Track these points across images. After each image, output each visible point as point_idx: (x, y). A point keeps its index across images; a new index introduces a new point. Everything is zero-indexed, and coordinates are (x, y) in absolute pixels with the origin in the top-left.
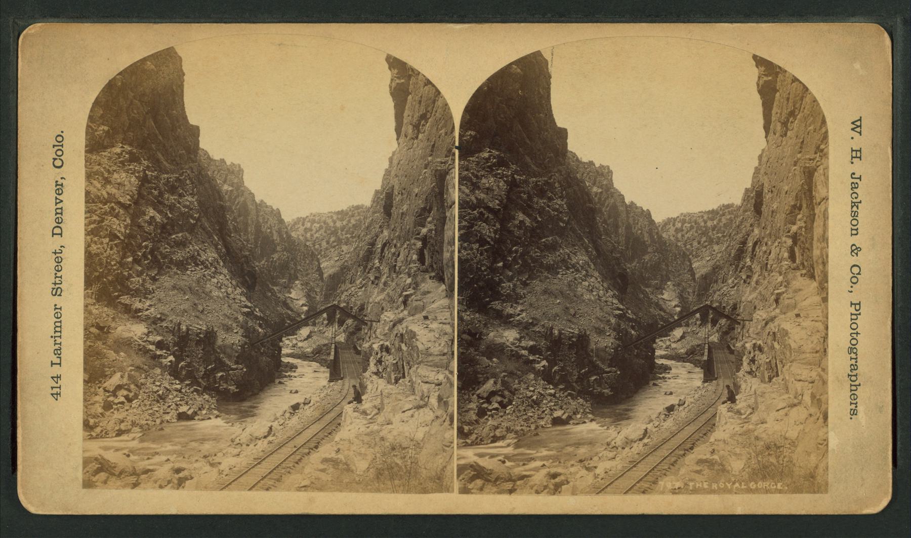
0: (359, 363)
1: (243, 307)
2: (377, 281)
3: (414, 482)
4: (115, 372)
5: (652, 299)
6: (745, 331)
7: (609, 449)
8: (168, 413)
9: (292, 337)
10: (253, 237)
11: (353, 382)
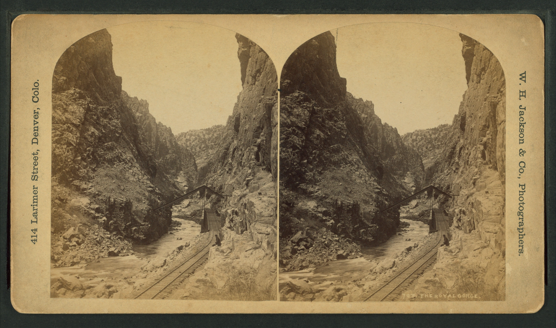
1: (148, 187)
2: (230, 172)
3: (252, 294)
5: (398, 182)
6: (454, 202)
7: (372, 274)
9: (178, 205)
11: (215, 233)
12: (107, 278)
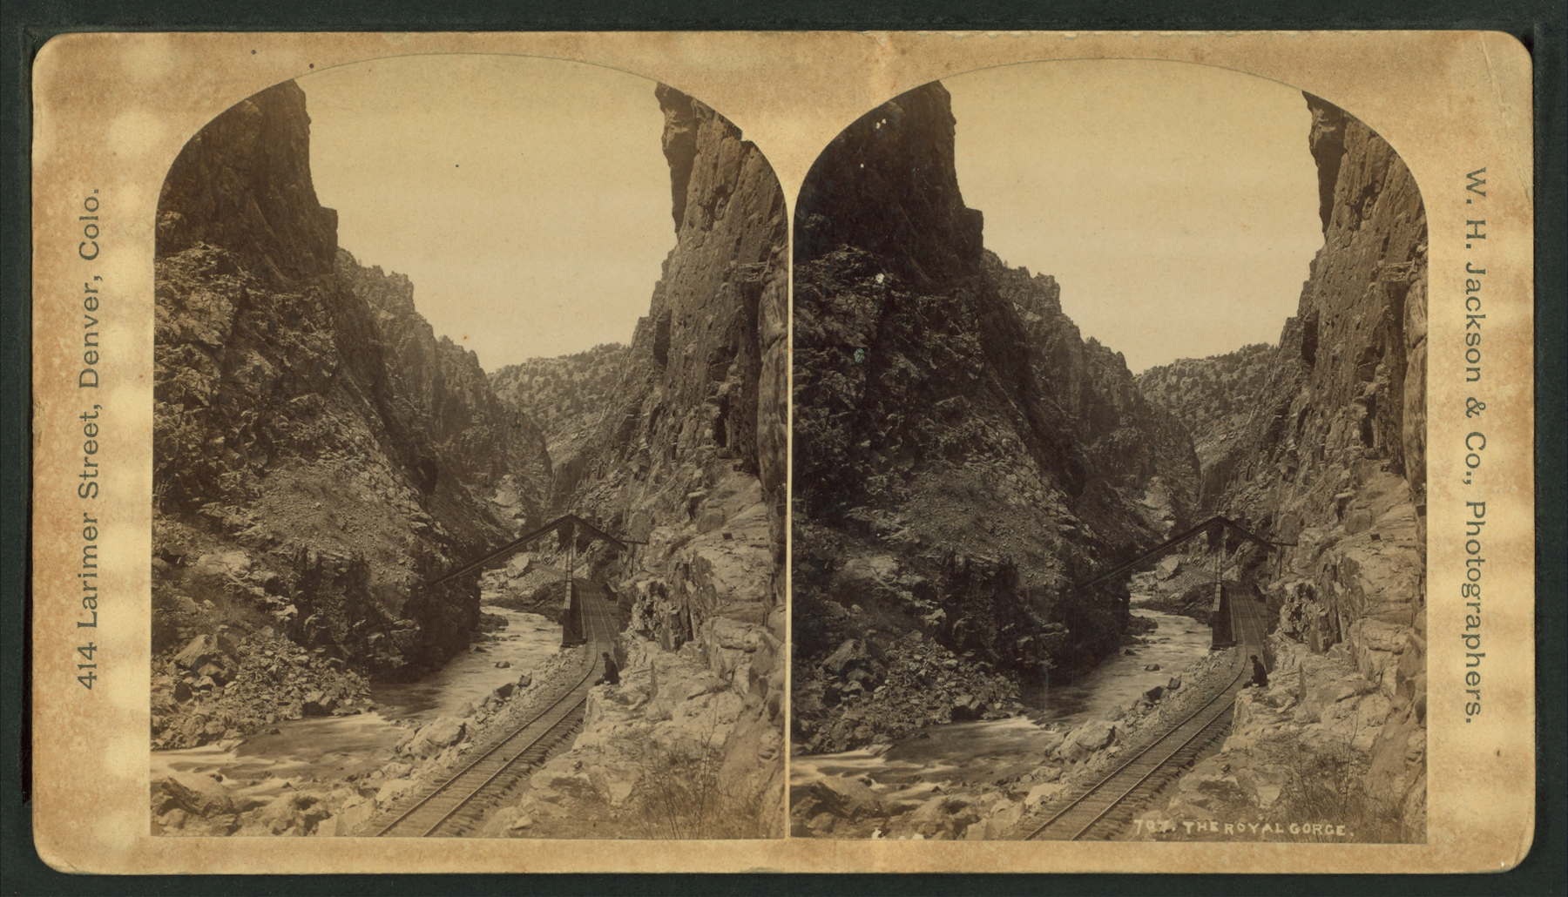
0: (613, 614)
2: (643, 475)
3: (711, 819)
4: (195, 634)
6: (1283, 562)
8: (287, 704)
9: (499, 571)
10: (1078, 401)
11: (604, 648)
12: (300, 778)
